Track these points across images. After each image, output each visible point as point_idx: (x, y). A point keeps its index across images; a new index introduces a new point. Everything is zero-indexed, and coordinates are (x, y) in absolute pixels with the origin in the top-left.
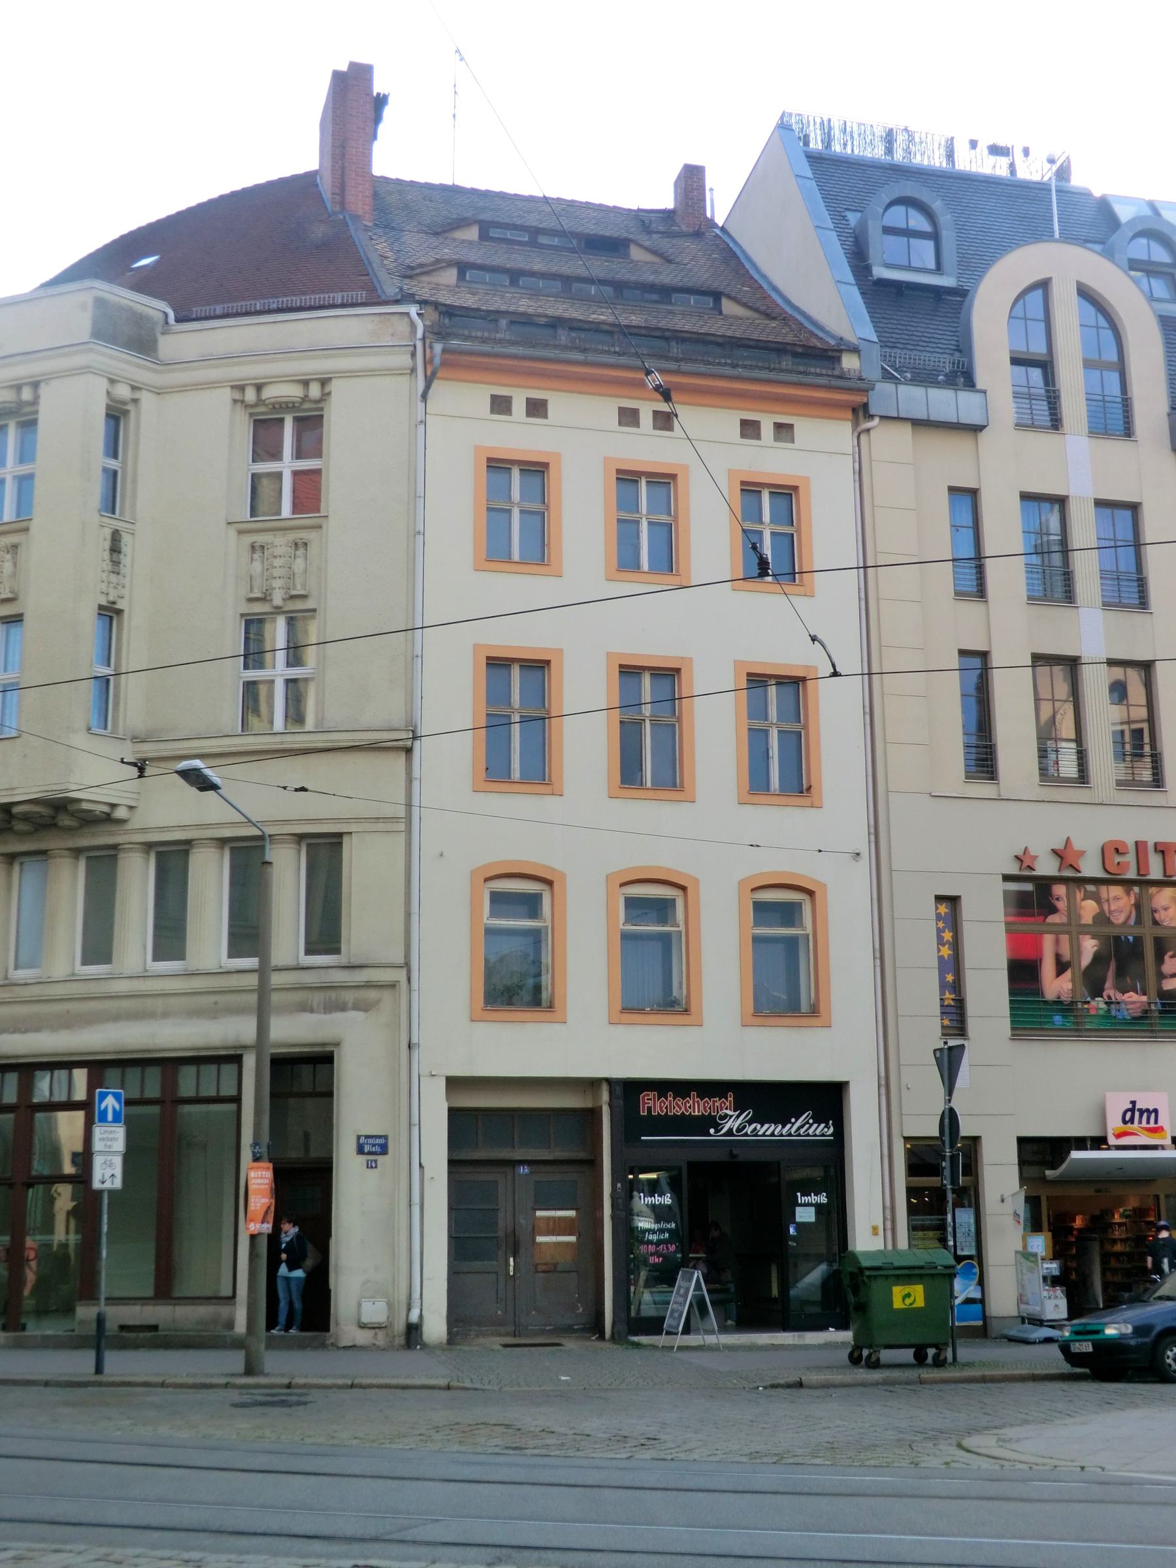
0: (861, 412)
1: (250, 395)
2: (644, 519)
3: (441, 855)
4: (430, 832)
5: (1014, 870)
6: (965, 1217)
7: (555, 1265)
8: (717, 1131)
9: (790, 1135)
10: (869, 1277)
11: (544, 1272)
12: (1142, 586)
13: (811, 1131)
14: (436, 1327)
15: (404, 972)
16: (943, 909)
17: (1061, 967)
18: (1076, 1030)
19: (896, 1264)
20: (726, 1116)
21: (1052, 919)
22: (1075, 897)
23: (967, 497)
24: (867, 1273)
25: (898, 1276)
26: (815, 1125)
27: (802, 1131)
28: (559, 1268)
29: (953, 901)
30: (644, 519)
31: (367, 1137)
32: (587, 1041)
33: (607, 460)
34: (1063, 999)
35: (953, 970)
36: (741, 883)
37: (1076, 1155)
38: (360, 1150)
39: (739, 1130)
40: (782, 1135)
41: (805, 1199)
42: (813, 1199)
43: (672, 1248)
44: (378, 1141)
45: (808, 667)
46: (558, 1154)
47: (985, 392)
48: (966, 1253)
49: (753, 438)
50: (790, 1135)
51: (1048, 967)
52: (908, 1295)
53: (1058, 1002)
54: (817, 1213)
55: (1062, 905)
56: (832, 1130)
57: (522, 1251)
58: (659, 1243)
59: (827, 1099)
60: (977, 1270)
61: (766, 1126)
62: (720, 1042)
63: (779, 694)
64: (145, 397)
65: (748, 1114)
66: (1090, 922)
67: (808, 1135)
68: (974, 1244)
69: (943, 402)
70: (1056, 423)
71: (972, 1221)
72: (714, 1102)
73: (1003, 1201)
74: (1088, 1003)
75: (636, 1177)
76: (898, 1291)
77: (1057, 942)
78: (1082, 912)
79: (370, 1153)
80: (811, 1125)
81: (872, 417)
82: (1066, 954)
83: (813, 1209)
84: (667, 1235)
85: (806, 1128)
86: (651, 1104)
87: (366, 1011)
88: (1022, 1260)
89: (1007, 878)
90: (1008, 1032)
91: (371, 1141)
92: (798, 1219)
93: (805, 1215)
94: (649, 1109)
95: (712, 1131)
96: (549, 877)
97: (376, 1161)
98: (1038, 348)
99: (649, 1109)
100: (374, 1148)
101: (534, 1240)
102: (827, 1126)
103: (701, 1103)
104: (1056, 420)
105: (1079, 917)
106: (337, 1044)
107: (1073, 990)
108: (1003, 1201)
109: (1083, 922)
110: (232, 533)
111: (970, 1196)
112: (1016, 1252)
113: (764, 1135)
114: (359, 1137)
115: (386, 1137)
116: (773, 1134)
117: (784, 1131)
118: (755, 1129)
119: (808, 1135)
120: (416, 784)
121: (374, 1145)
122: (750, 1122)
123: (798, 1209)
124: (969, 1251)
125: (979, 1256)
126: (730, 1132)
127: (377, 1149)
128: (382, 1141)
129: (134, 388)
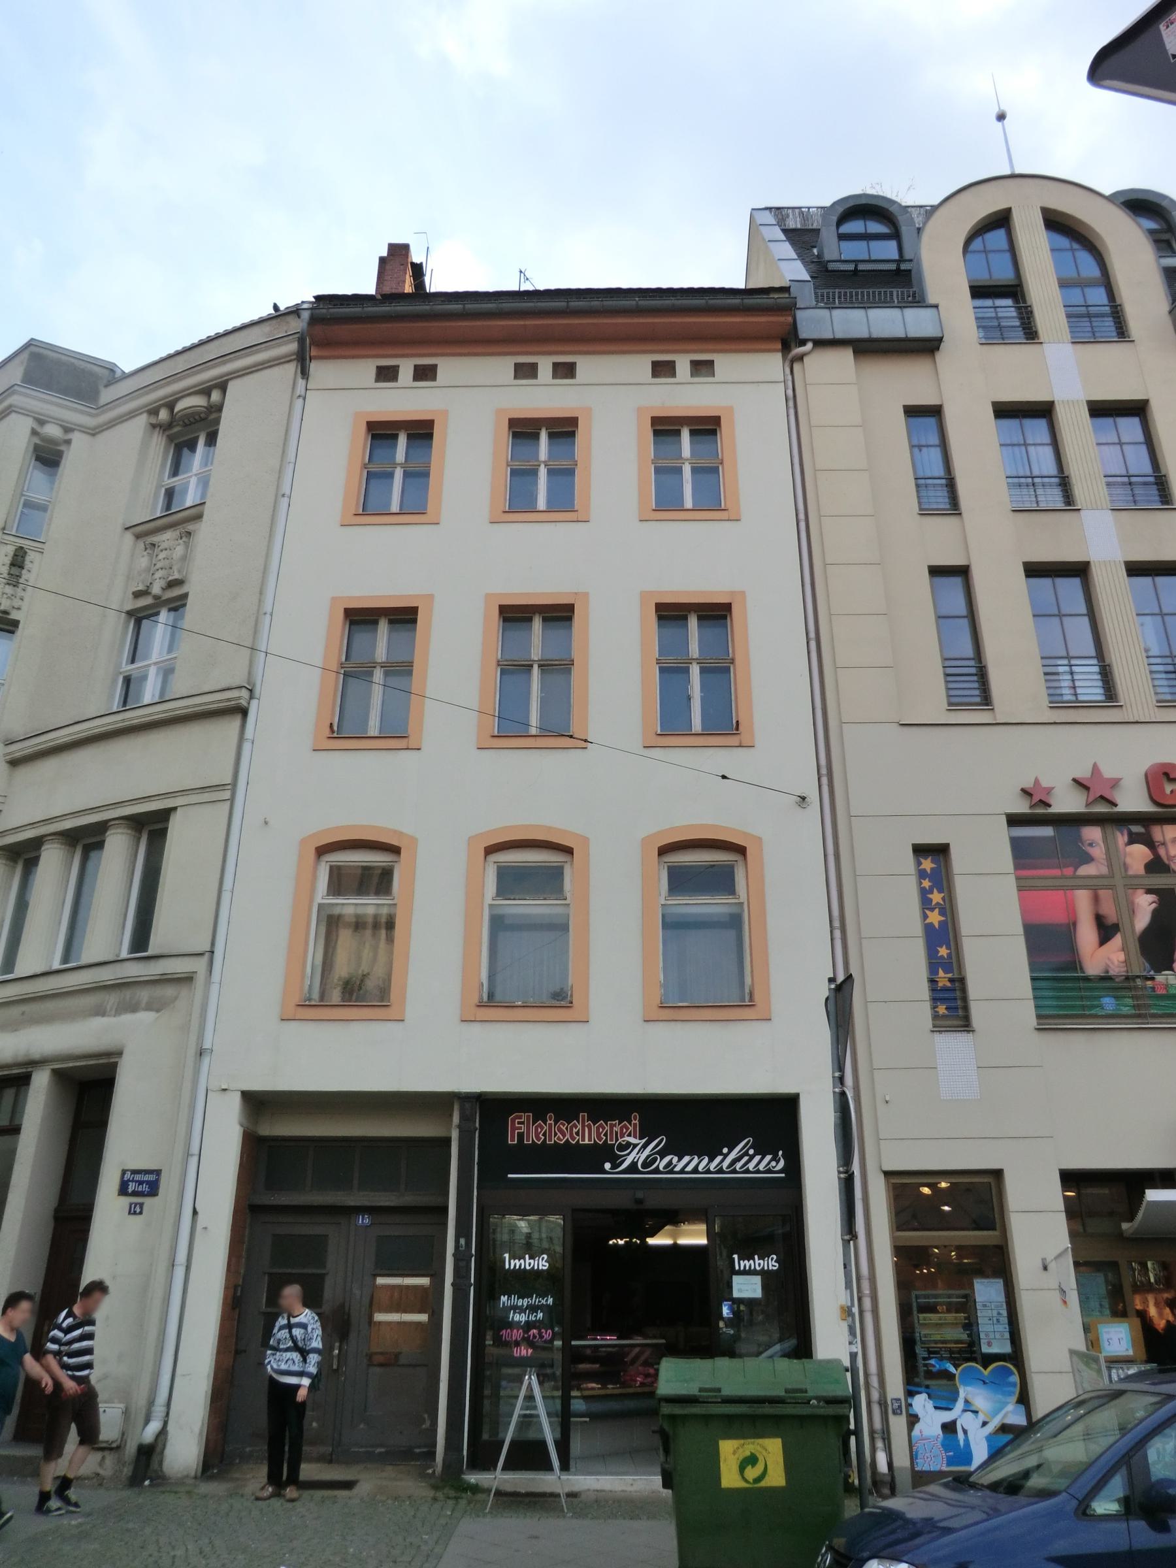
0: (788, 341)
1: (164, 415)
2: (542, 466)
3: (266, 823)
4: (254, 798)
5: (1022, 807)
6: (987, 1292)
7: (397, 1356)
8: (615, 1166)
9: (721, 1171)
10: (673, 1418)
11: (381, 1365)
12: (1164, 490)
13: (751, 1166)
14: (184, 1451)
15: (204, 960)
16: (928, 864)
17: (1106, 931)
18: (1139, 1016)
19: (727, 1391)
20: (629, 1144)
21: (1085, 870)
22: (1116, 843)
23: (925, 414)
24: (666, 1409)
25: (729, 1418)
26: (758, 1158)
27: (738, 1165)
28: (402, 1361)
29: (940, 851)
30: (542, 466)
31: (134, 1172)
32: (434, 1043)
33: (499, 412)
34: (1111, 973)
35: (943, 940)
36: (646, 841)
37: (1153, 1195)
38: (123, 1190)
39: (646, 1164)
40: (708, 1172)
41: (746, 1264)
42: (757, 1263)
43: (547, 1335)
44: (147, 1178)
45: (732, 592)
46: (408, 1199)
47: (936, 306)
48: (995, 1350)
49: (665, 376)
50: (721, 1171)
51: (1087, 934)
52: (752, 1460)
53: (1106, 978)
54: (765, 1287)
55: (1098, 852)
56: (782, 1164)
57: (353, 1336)
58: (529, 1325)
59: (771, 1120)
60: (1015, 1378)
61: (686, 1159)
62: (618, 1042)
63: (695, 625)
64: (76, 437)
65: (660, 1141)
66: (1142, 871)
67: (747, 1171)
68: (1007, 1335)
69: (886, 322)
70: (1030, 333)
71: (1001, 1298)
72: (612, 1126)
73: (1045, 1268)
74: (1152, 979)
75: (644, 1242)
76: (730, 1451)
77: (1096, 899)
78: (1128, 860)
79: (135, 1194)
80: (752, 1158)
81: (803, 342)
82: (1109, 911)
83: (758, 1280)
84: (540, 1315)
85: (742, 1161)
86: (523, 1129)
87: (158, 1011)
88: (1082, 1367)
89: (1014, 820)
90: (1033, 1021)
91: (138, 1177)
92: (736, 1294)
93: (747, 1287)
94: (521, 1136)
95: (607, 1166)
96: (394, 842)
97: (141, 1205)
98: (1002, 274)
99: (521, 1136)
100: (142, 1186)
101: (371, 1317)
102: (775, 1159)
103: (594, 1129)
104: (1031, 333)
105: (1126, 867)
106: (120, 1054)
107: (1127, 962)
108: (1045, 1268)
109: (1131, 872)
110: (129, 537)
111: (996, 1260)
112: (1072, 1352)
113: (682, 1171)
114: (124, 1172)
115: (158, 1172)
116: (695, 1171)
117: (712, 1166)
118: (670, 1163)
119: (747, 1171)
120: (247, 747)
121: (141, 1183)
122: (663, 1154)
123: (736, 1280)
124: (1002, 1346)
125: (1016, 1357)
126: (633, 1168)
127: (145, 1188)
128: (152, 1177)
129: (67, 430)
